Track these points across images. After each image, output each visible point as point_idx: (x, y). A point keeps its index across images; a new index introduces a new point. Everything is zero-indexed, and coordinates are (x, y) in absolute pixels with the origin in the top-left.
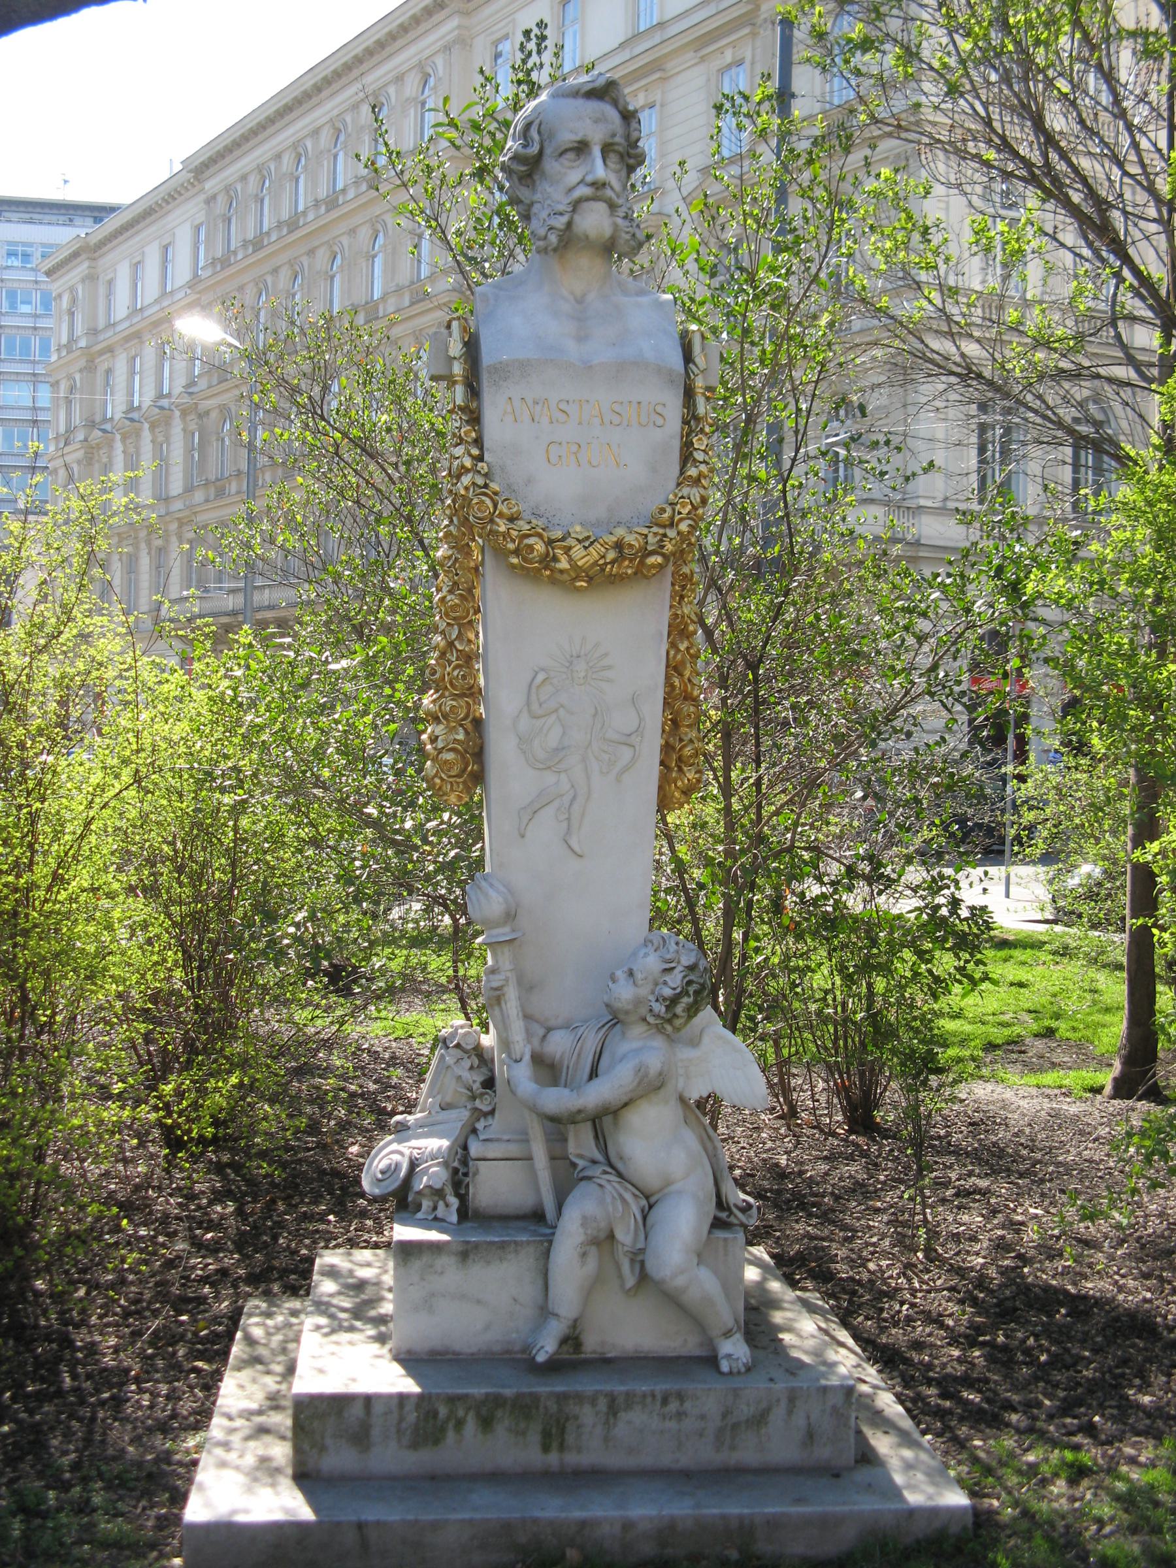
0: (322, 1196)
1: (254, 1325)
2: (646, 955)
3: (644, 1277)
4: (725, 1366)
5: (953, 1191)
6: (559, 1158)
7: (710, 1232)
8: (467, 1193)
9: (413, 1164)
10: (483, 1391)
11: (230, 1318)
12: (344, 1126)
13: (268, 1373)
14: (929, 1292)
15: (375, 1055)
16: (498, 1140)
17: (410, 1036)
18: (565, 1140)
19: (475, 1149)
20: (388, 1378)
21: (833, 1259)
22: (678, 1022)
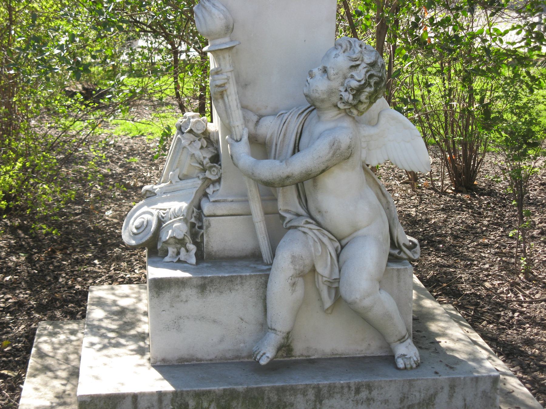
0: (88, 247)
1: (43, 343)
2: (336, 56)
3: (338, 299)
4: (401, 363)
5: (539, 231)
6: (272, 214)
7: (387, 265)
8: (202, 242)
9: (160, 222)
10: (221, 388)
11: (27, 337)
12: (101, 197)
13: (56, 377)
14: (531, 303)
15: (119, 148)
16: (224, 201)
17: (142, 135)
18: (276, 200)
19: (207, 208)
20: (153, 382)
21: (459, 281)
22: (362, 107)
